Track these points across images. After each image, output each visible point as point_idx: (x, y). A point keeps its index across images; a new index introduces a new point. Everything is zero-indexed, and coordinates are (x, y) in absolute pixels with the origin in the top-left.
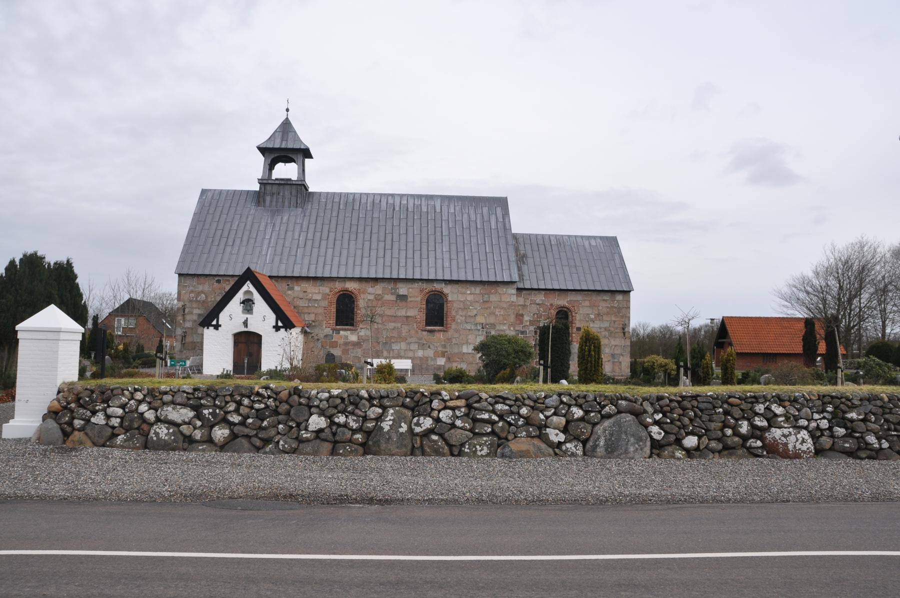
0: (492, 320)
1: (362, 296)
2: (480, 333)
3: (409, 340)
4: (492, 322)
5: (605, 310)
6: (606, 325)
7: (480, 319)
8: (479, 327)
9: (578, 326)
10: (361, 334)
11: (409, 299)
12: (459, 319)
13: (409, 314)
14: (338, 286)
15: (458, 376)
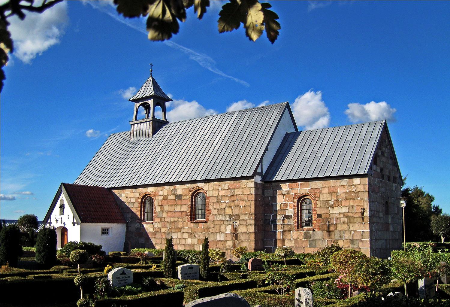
0: (236, 211)
1: (157, 198)
2: (229, 223)
3: (183, 231)
4: (237, 213)
5: (343, 196)
6: (344, 210)
7: (228, 211)
8: (228, 218)
9: (319, 213)
10: (156, 226)
11: (183, 198)
12: (215, 212)
13: (182, 210)
14: (144, 190)
15: (356, 169)
